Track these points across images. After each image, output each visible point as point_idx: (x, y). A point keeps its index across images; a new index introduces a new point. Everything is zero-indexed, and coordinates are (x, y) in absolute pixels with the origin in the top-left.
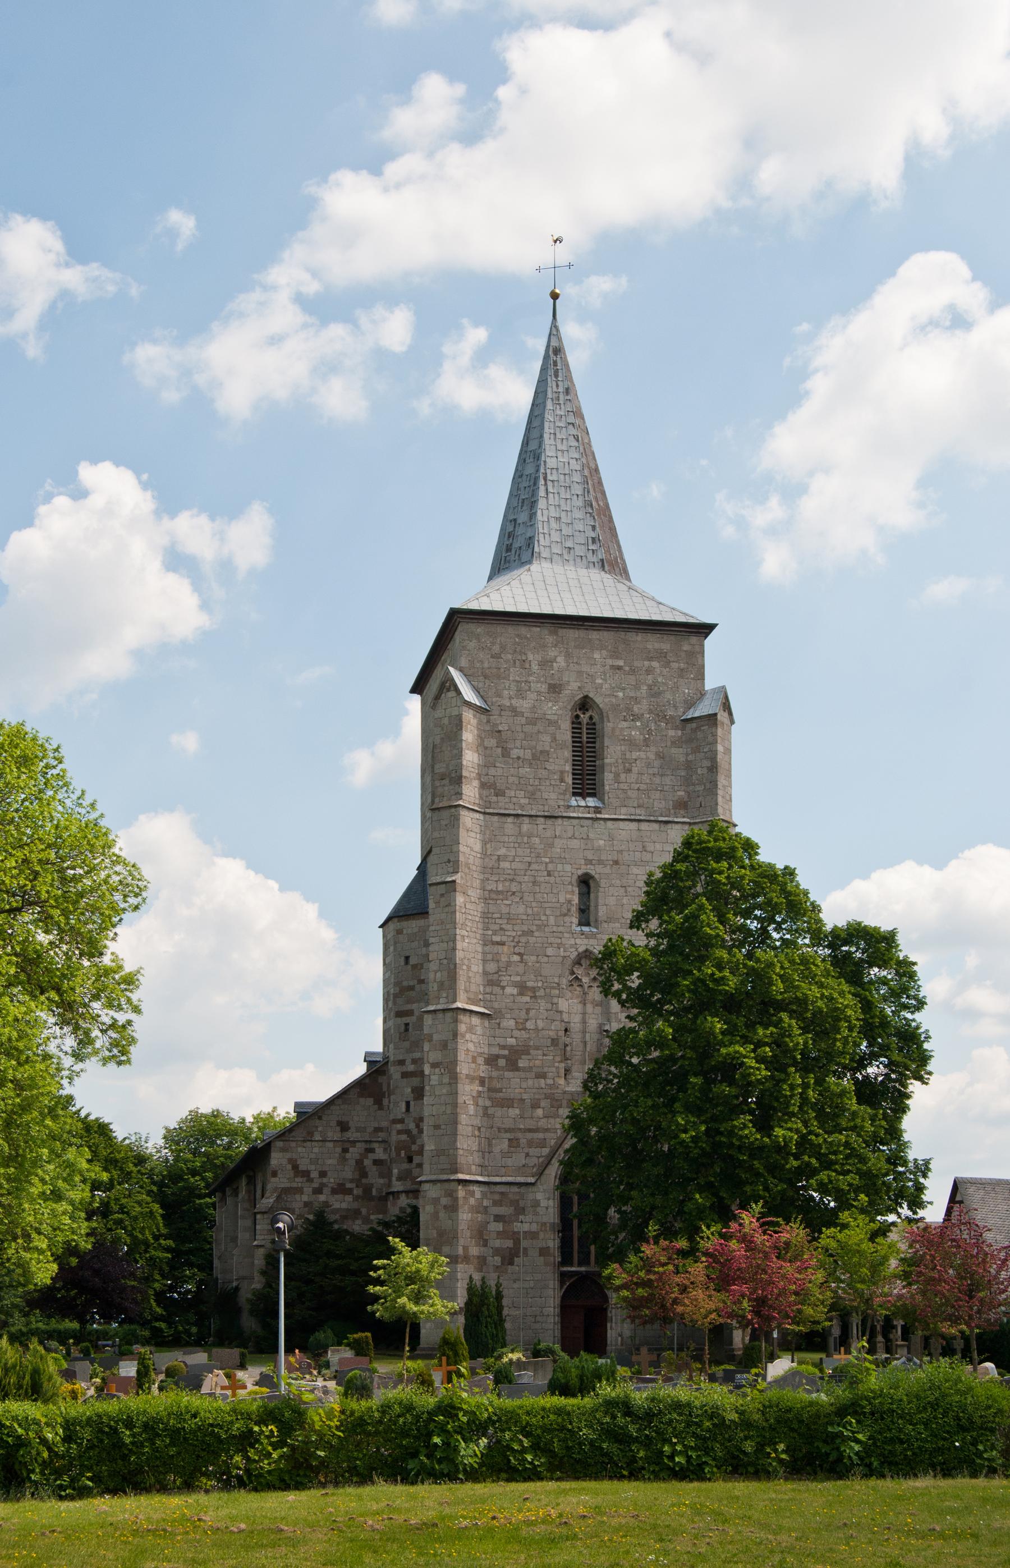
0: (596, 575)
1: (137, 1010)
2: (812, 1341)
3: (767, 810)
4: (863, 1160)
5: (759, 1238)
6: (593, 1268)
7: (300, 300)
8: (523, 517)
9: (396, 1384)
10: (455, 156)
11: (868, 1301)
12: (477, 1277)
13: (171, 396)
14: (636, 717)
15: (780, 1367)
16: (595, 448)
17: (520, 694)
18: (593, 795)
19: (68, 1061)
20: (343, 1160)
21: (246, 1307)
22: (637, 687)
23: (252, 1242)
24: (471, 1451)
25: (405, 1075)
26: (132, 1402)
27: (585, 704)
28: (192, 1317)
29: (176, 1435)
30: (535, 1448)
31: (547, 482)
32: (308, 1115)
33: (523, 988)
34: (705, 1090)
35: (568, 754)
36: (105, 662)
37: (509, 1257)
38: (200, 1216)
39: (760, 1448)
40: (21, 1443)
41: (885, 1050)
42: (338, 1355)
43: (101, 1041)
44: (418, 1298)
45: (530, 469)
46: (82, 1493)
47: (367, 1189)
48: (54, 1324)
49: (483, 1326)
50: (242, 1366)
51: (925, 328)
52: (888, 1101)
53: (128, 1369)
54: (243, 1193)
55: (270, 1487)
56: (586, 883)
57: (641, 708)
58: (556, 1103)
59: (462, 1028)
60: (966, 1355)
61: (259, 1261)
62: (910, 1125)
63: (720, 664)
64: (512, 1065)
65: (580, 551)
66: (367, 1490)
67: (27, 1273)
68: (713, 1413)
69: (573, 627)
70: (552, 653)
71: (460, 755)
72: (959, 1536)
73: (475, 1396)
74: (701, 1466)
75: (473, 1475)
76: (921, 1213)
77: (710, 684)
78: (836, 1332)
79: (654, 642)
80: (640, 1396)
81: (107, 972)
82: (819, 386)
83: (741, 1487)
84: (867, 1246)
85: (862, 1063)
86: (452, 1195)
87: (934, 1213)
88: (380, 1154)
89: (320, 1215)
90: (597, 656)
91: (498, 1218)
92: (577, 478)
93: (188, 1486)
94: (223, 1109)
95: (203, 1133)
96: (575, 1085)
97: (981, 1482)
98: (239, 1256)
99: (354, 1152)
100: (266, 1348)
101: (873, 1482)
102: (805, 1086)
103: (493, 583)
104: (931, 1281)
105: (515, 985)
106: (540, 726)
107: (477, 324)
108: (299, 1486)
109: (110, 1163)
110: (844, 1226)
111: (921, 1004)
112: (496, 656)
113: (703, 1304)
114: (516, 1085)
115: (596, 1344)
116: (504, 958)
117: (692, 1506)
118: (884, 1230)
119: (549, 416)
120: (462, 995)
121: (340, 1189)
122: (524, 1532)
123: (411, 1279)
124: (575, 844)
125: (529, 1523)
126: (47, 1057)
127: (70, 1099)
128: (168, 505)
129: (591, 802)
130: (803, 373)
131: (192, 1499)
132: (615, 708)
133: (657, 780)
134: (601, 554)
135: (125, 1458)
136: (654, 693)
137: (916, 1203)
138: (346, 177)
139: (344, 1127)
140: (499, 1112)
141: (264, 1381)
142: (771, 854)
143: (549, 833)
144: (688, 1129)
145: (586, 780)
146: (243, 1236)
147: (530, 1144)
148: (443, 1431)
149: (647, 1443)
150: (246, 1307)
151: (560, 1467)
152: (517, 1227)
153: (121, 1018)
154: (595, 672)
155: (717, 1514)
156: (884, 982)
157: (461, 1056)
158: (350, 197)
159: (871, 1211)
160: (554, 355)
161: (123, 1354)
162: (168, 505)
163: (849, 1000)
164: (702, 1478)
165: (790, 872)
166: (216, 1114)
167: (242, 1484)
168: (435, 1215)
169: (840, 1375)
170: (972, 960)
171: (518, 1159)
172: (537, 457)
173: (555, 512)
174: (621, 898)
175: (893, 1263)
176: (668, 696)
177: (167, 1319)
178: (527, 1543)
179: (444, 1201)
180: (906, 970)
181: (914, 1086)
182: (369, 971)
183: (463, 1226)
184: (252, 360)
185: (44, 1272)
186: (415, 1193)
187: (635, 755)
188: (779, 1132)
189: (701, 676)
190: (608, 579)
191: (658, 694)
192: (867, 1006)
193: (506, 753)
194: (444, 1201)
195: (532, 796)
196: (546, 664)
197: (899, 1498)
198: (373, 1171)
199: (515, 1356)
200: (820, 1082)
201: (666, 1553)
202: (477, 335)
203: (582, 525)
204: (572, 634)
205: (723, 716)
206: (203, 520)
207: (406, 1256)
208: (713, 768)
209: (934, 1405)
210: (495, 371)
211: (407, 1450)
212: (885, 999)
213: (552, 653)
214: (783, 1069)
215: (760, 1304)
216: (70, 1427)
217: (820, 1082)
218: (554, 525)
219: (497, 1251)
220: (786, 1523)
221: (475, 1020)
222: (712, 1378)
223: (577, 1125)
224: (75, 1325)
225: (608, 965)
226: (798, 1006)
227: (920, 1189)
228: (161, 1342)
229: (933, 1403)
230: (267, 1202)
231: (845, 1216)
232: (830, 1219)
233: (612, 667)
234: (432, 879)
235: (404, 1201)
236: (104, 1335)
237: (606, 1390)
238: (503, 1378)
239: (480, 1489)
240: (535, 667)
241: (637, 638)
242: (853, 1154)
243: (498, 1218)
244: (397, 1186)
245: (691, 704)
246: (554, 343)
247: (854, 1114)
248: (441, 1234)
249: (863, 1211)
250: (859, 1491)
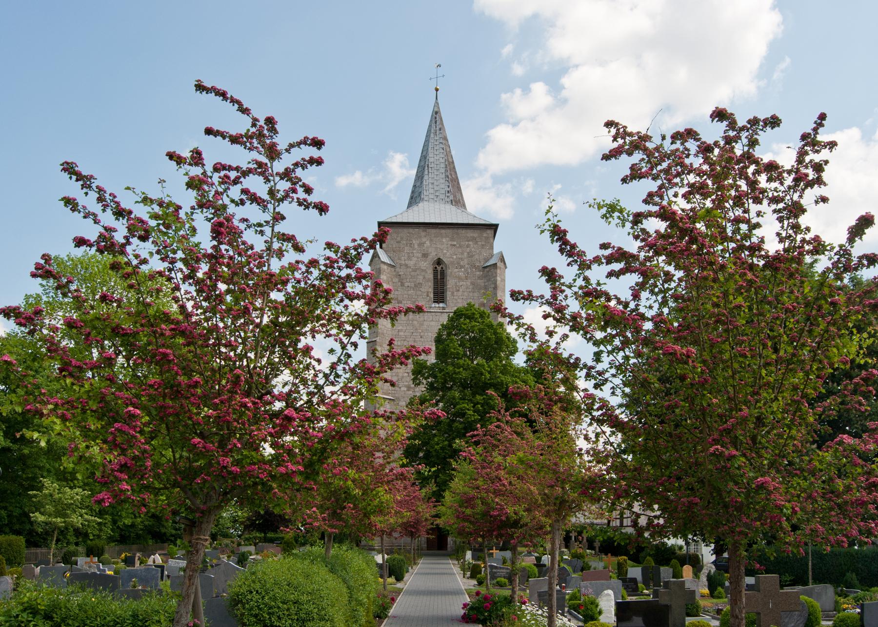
0: (448, 206)
8: (418, 184)
14: (462, 267)
16: (453, 153)
17: (409, 258)
18: (443, 302)
22: (462, 254)
27: (439, 262)
57: (464, 263)
69: (433, 228)
70: (424, 240)
77: (496, 251)
79: (470, 233)
90: (444, 240)
92: (443, 165)
105: (405, 386)
106: (418, 272)
112: (399, 242)
116: (401, 375)
119: (431, 141)
129: (441, 305)
132: (452, 263)
133: (471, 294)
134: (451, 197)
136: (470, 255)
143: (422, 319)
154: (443, 247)
173: (435, 180)
176: (477, 257)
187: (461, 283)
189: (492, 248)
191: (472, 256)
193: (402, 285)
196: (421, 244)
204: (433, 231)
205: (500, 264)
213: (424, 240)
218: (431, 186)
233: (452, 245)
240: (416, 246)
241: (463, 232)
245: (487, 260)
246: (436, 109)
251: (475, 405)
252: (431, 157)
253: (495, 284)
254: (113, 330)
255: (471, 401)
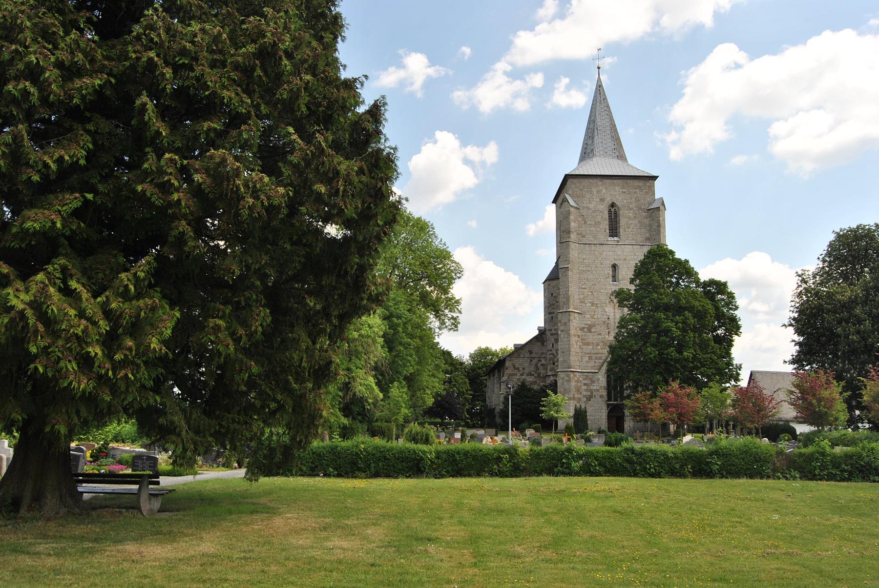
0: (616, 161)
1: (460, 312)
2: (698, 429)
3: (678, 241)
4: (717, 364)
5: (679, 391)
6: (619, 402)
7: (505, 73)
8: (590, 142)
9: (548, 441)
10: (558, 23)
11: (720, 415)
12: (578, 405)
13: (465, 107)
14: (631, 209)
15: (688, 438)
17: (590, 202)
19: (437, 330)
20: (530, 364)
21: (497, 415)
22: (631, 198)
23: (498, 394)
24: (576, 465)
25: (552, 334)
26: (460, 446)
27: (613, 205)
28: (479, 418)
29: (475, 457)
30: (600, 464)
31: (600, 129)
32: (519, 349)
33: (593, 304)
34: (658, 339)
35: (607, 222)
36: (445, 197)
37: (589, 398)
38: (481, 383)
39: (681, 466)
40: (422, 459)
41: (724, 325)
42: (529, 432)
43: (448, 323)
44: (557, 412)
45: (592, 126)
46: (443, 476)
47: (539, 374)
48: (433, 420)
49: (580, 420)
50: (496, 435)
51: (728, 68)
52: (726, 343)
53: (458, 435)
54: (496, 375)
55: (507, 476)
56: (614, 267)
58: (604, 344)
59: (572, 318)
60: (757, 434)
61: (502, 399)
62: (735, 352)
63: (660, 190)
64: (590, 331)
65: (610, 153)
66: (541, 478)
67: (424, 402)
68: (665, 454)
70: (601, 188)
71: (569, 224)
72: (757, 500)
73: (578, 445)
74: (660, 473)
75: (577, 474)
76: (739, 383)
77: (657, 197)
78: (708, 426)
79: (637, 183)
80: (637, 446)
81: (451, 299)
82: (688, 91)
83: (675, 481)
84: (719, 394)
85: (715, 329)
86: (568, 376)
87: (744, 383)
88: (543, 362)
89: (523, 384)
91: (585, 384)
92: (608, 128)
93: (479, 475)
94: (489, 346)
95: (482, 355)
96: (611, 338)
97: (764, 481)
98: (501, 396)
99: (535, 361)
100: (505, 429)
101: (723, 480)
102: (694, 337)
103: (581, 164)
104: (743, 407)
107: (565, 77)
108: (516, 476)
109: (452, 364)
110: (711, 387)
111: (737, 308)
113: (658, 414)
114: (590, 338)
115: (620, 429)
117: (657, 487)
118: (726, 389)
119: (598, 108)
120: (571, 306)
121: (530, 374)
122: (596, 494)
123: (555, 405)
124: (610, 253)
125: (598, 491)
126: (430, 329)
127: (438, 343)
128: (464, 143)
129: (616, 239)
130: (684, 87)
131: (480, 479)
132: (623, 206)
134: (617, 154)
135: (457, 465)
136: (637, 200)
137: (737, 380)
138: (522, 33)
139: (531, 352)
140: (585, 347)
141: (503, 440)
142: (680, 255)
144: (652, 352)
145: (614, 231)
146: (496, 390)
147: (596, 358)
148: (567, 458)
149: (640, 464)
150: (497, 415)
151: (608, 472)
152: (592, 387)
153: (455, 315)
154: (615, 194)
155: (666, 490)
156: (723, 300)
157: (571, 328)
158: (523, 39)
159: (720, 382)
160: (599, 86)
161: (456, 430)
162: (464, 143)
163: (710, 306)
164: (660, 477)
165: (687, 261)
166: (487, 348)
167: (497, 475)
168: (563, 384)
169: (710, 441)
170: (754, 292)
171: (592, 364)
172: (594, 122)
173: (602, 140)
174: (627, 272)
175: (729, 401)
177: (471, 419)
178: (597, 498)
179: (566, 378)
180: (731, 296)
181: (735, 337)
182: (538, 299)
183: (573, 387)
184: (492, 94)
185: (430, 401)
186: (556, 375)
188: (685, 353)
190: (620, 162)
192: (717, 308)
193: (585, 223)
194: (566, 378)
195: (595, 237)
196: (599, 192)
197: (734, 486)
198: (541, 368)
199: (591, 433)
200: (700, 335)
201: (648, 503)
202: (565, 81)
203: (611, 145)
204: (608, 181)
206: (475, 148)
207: (553, 397)
208: (659, 226)
209: (746, 452)
210: (573, 92)
211: (554, 464)
212: (723, 306)
214: (686, 331)
215: (680, 415)
216: (438, 453)
217: (700, 335)
219: (585, 396)
220: (691, 494)
221: (576, 315)
222: (663, 442)
223: (612, 349)
224: (439, 420)
225: (621, 297)
226: (691, 309)
227: (738, 374)
228: (469, 427)
229: (746, 451)
230: (505, 378)
231: (711, 384)
232: (705, 385)
234: (560, 267)
235: (552, 378)
236: (450, 424)
237: (625, 445)
238: (588, 440)
239: (580, 479)
242: (713, 361)
243: (585, 384)
244: (549, 373)
245: (650, 204)
247: (713, 347)
248: (565, 390)
249: (717, 382)
250: (718, 482)
251: (677, 323)
252: (599, 121)
253: (659, 223)
254: (581, 302)
255: (672, 321)
